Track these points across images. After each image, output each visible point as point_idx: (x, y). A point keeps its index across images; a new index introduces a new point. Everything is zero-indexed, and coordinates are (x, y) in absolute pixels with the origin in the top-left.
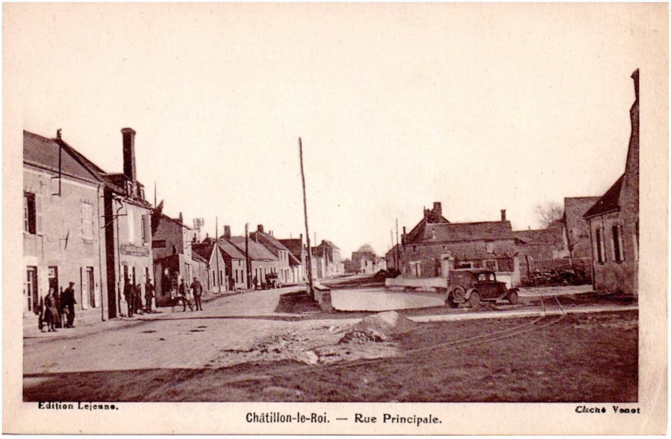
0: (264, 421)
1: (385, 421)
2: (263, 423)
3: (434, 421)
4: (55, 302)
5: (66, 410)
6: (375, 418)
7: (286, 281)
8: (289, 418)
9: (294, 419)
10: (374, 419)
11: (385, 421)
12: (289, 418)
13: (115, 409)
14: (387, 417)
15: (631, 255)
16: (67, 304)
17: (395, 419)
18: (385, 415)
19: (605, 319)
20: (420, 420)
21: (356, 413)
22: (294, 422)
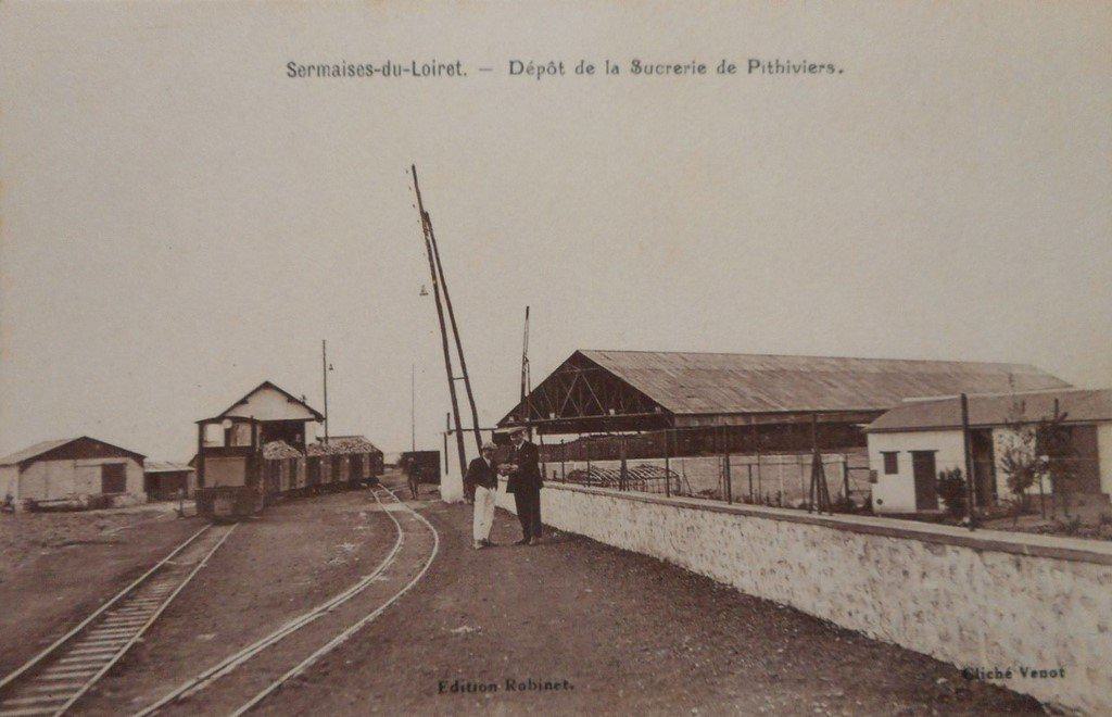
0: (339, 74)
1: (750, 72)
2: (338, 78)
3: (699, 71)
4: (713, 428)
5: (454, 77)
6: (593, 68)
7: (818, 468)
8: (397, 73)
9: (407, 70)
10: (370, 70)
11: (750, 72)
12: (397, 73)
13: (836, 73)
14: (754, 64)
15: (731, 439)
16: (612, 408)
17: (689, 67)
18: (750, 61)
19: (127, 576)
20: (541, 70)
21: (513, 60)
22: (378, 76)
